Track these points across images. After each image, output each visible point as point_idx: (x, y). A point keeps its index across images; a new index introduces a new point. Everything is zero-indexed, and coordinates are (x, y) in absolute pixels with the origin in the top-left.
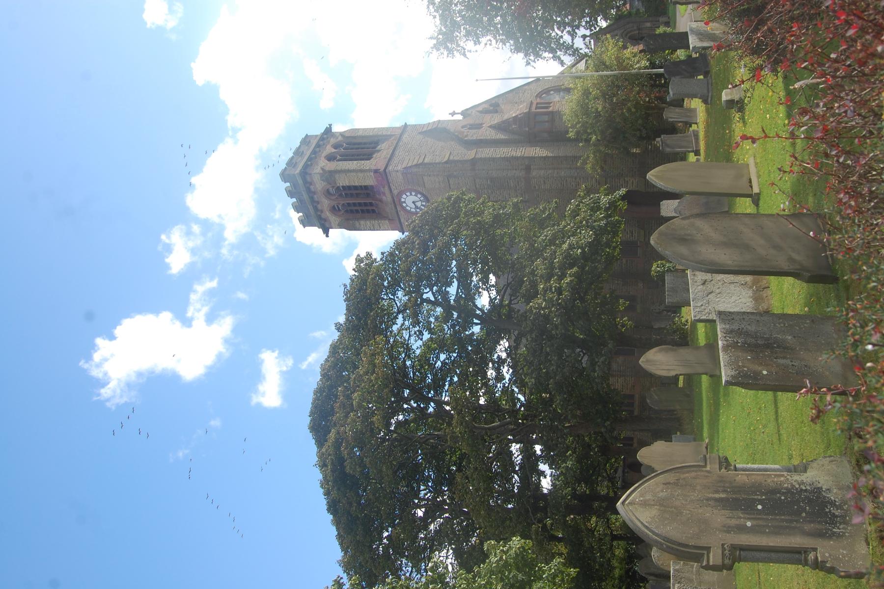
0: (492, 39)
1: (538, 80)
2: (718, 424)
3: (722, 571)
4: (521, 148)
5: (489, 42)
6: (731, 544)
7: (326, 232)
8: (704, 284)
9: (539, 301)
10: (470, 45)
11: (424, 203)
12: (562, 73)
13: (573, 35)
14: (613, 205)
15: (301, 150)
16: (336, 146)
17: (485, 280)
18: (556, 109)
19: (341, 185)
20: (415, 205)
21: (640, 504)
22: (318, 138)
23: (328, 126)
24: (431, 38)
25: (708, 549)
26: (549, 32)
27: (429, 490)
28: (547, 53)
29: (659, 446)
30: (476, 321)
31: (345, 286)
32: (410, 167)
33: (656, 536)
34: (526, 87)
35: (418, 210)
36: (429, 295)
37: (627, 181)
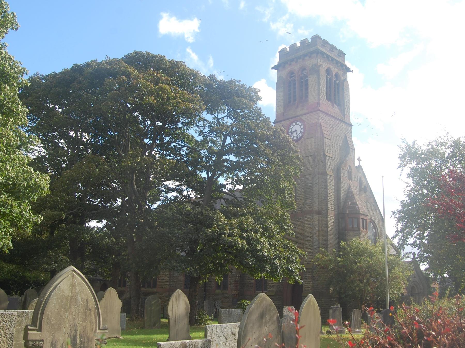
0: (411, 187)
1: (383, 220)
2: (132, 345)
3: (24, 339)
4: (334, 208)
5: (409, 185)
6: (43, 346)
7: (275, 68)
8: (233, 333)
9: (223, 220)
10: (407, 170)
11: (295, 138)
12: (387, 237)
13: (414, 245)
14: (290, 272)
15: (334, 50)
16: (337, 75)
17: (239, 181)
18: (362, 233)
19: (309, 79)
20: (294, 132)
21: (72, 283)
22: (343, 62)
23: (351, 70)
24: (414, 143)
25: (40, 330)
26: (416, 227)
27: (88, 140)
28: (401, 226)
29: (118, 304)
30: (210, 175)
31: (239, 81)
32: (321, 128)
33: (50, 293)
34: (378, 212)
35: (290, 134)
36: (228, 141)
37: (309, 284)
